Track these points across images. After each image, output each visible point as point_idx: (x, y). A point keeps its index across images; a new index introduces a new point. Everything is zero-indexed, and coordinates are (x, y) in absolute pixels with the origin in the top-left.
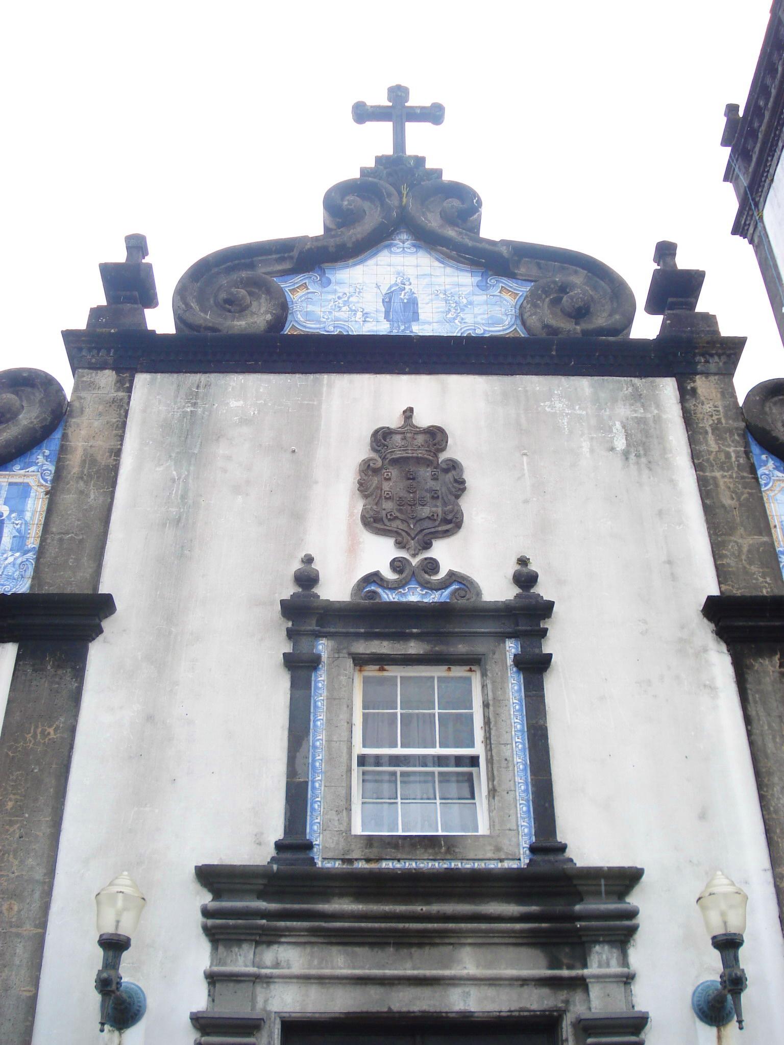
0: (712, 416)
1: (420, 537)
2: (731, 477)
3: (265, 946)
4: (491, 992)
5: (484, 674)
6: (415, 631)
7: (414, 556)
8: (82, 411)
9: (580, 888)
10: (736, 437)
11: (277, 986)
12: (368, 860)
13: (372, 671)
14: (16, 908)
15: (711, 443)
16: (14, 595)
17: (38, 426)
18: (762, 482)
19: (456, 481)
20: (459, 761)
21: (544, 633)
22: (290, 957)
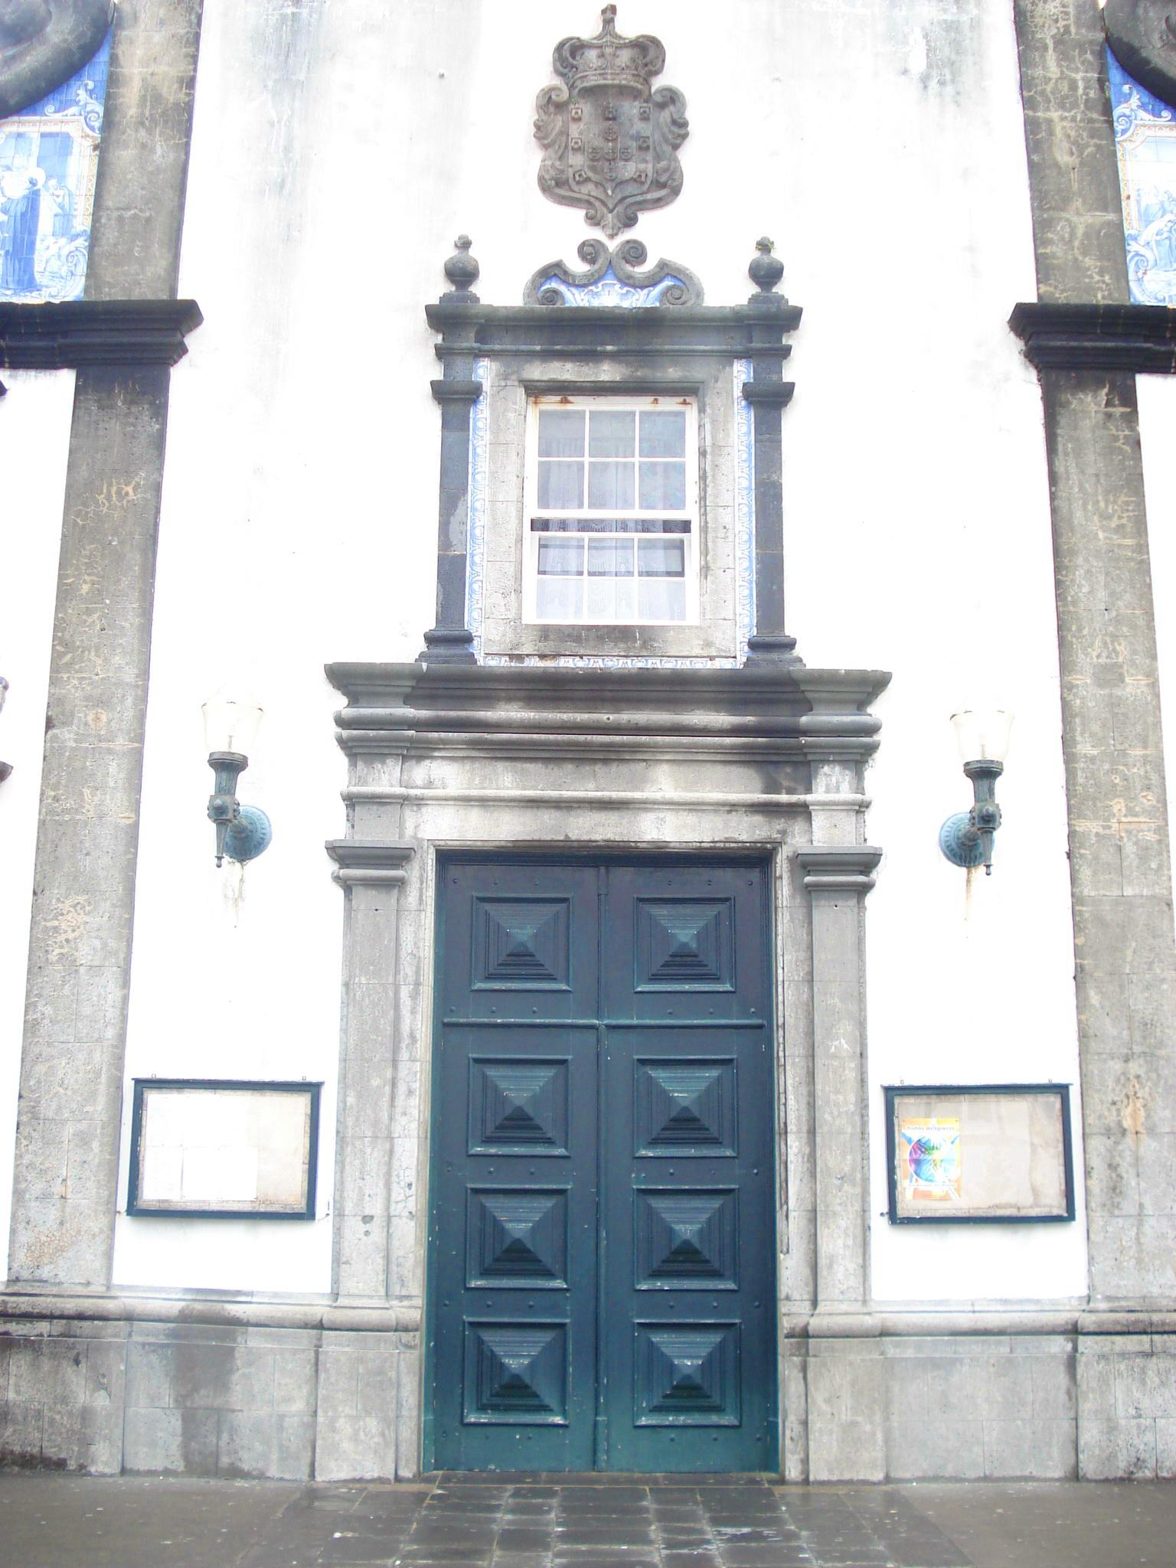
0: (1057, 21)
1: (620, 209)
2: (1074, 119)
3: (414, 762)
4: (691, 819)
5: (702, 410)
6: (609, 348)
7: (612, 237)
8: (136, 18)
9: (809, 695)
10: (1089, 56)
11: (430, 809)
12: (542, 657)
13: (551, 403)
14: (104, 718)
15: (1051, 66)
16: (65, 305)
17: (74, 47)
18: (1118, 127)
19: (674, 122)
20: (668, 526)
21: (786, 352)
22: (446, 775)
